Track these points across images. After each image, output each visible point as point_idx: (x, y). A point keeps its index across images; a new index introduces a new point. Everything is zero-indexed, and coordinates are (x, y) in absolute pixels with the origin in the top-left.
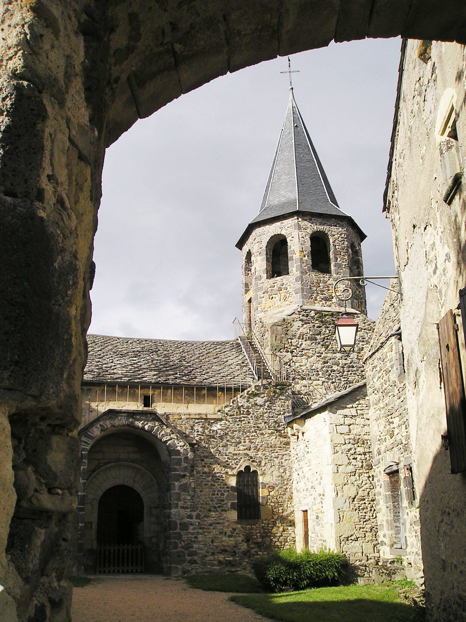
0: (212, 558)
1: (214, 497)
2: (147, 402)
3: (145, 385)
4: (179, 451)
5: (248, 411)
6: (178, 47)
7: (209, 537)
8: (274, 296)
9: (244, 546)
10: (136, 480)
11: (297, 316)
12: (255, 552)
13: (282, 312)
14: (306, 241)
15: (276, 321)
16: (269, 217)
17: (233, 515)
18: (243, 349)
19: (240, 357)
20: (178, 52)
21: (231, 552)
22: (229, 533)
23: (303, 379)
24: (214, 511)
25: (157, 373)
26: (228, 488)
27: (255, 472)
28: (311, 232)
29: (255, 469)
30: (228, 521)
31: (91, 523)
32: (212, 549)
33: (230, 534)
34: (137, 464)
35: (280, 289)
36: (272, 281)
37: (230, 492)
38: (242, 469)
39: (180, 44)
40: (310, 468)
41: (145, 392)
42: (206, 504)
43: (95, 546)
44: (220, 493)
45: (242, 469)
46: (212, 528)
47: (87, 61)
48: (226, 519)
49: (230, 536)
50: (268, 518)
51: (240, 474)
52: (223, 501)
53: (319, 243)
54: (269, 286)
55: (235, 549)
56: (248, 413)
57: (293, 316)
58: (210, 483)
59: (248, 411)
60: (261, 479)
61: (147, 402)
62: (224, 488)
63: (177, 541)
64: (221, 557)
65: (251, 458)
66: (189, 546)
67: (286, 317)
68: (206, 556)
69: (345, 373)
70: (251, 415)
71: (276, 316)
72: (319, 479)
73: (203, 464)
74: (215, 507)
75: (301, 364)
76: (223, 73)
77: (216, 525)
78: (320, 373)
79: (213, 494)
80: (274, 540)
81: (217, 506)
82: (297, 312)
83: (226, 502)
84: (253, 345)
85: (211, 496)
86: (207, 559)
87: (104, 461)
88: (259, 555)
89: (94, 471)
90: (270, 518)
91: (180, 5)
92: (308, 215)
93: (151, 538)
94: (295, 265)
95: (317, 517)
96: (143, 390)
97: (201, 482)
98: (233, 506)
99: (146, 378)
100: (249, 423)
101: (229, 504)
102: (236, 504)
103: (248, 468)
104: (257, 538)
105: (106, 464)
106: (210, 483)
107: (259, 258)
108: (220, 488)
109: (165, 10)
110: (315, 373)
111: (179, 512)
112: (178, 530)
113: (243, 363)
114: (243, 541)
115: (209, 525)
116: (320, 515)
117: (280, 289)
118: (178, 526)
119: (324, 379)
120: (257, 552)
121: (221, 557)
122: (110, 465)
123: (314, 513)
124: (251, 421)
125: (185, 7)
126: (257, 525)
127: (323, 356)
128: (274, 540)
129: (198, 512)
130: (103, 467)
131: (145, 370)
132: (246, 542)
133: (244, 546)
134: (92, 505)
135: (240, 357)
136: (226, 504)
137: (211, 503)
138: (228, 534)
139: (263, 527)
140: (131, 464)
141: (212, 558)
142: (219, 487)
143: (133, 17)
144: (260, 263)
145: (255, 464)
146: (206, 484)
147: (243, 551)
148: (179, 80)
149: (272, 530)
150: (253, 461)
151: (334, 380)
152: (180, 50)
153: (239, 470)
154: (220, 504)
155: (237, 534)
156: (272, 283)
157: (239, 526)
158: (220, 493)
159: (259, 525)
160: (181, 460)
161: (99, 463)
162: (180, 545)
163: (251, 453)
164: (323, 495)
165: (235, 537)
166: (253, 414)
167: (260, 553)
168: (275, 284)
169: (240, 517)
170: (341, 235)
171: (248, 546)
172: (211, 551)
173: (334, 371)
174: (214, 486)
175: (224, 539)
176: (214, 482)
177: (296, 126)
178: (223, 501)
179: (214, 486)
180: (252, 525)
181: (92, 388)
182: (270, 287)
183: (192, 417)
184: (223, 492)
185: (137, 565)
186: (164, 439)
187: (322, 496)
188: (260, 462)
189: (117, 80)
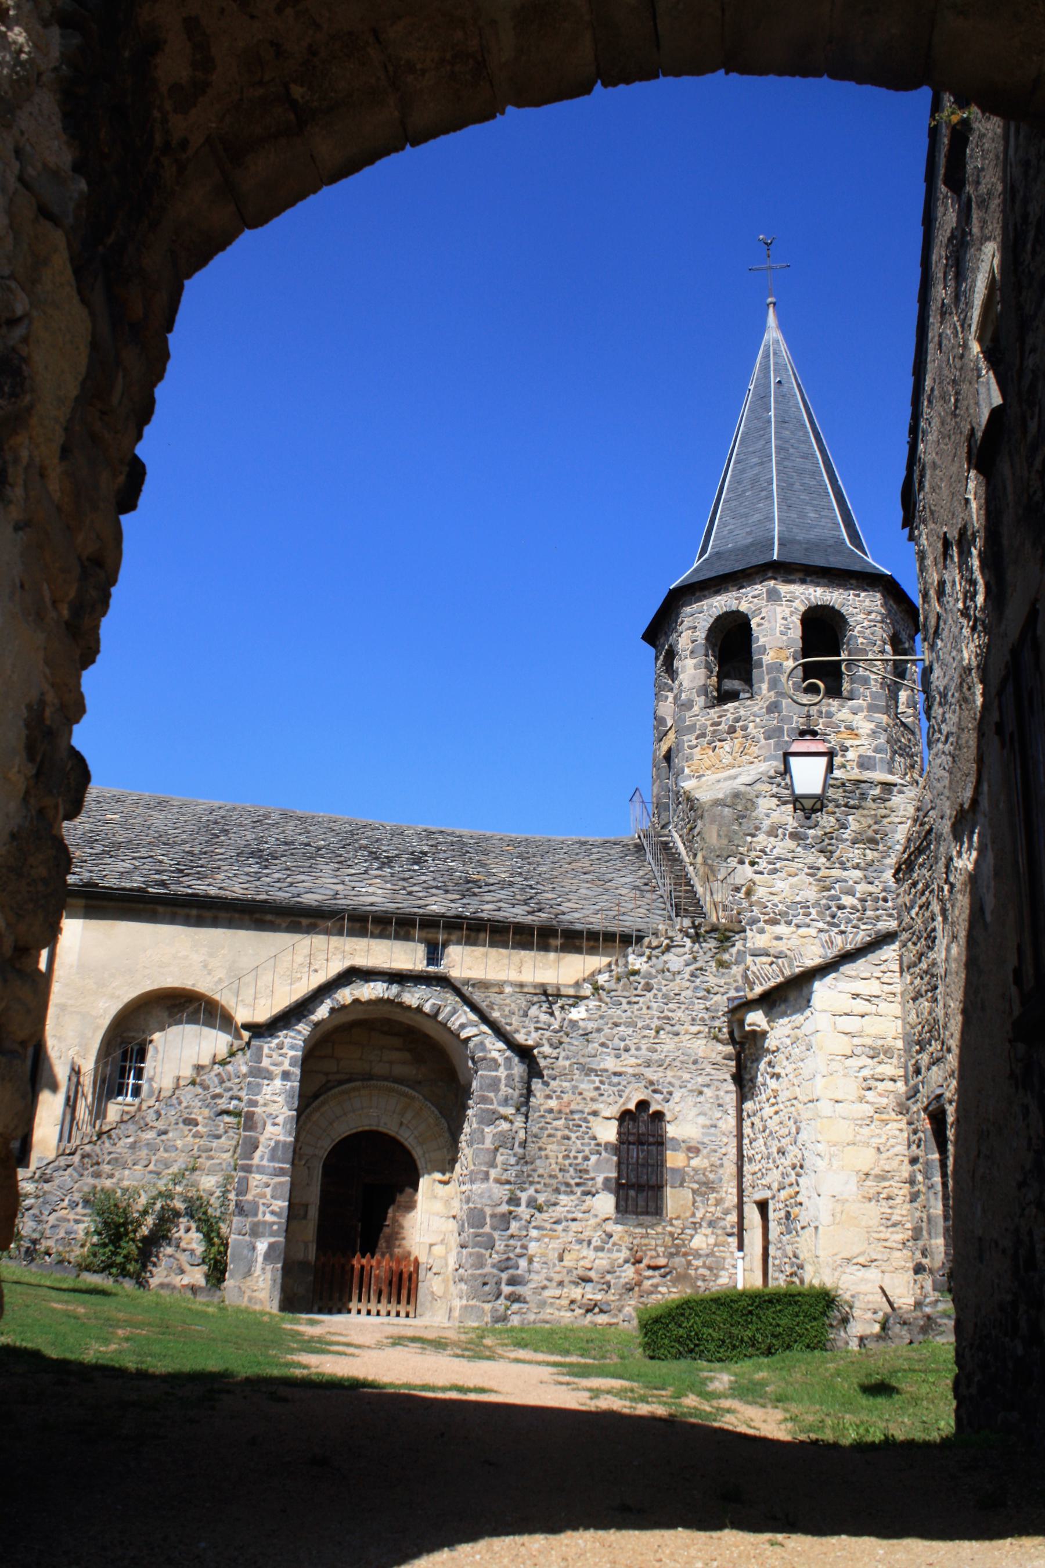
0: (557, 1292)
1: (567, 1162)
2: (434, 955)
3: (430, 923)
4: (495, 1060)
5: (647, 984)
6: (297, 91)
7: (553, 1249)
8: (718, 744)
9: (629, 1273)
10: (405, 1122)
11: (766, 787)
12: (652, 1285)
13: (735, 778)
14: (791, 626)
15: (721, 796)
16: (713, 574)
17: (605, 1203)
18: (649, 856)
19: (641, 873)
20: (300, 100)
21: (598, 1283)
22: (596, 1242)
23: (774, 922)
24: (566, 1193)
25: (458, 897)
26: (599, 1145)
27: (659, 1116)
28: (803, 609)
29: (659, 1108)
30: (596, 1216)
31: (307, 1206)
32: (559, 1273)
33: (599, 1243)
34: (408, 1086)
35: (732, 730)
36: (714, 713)
37: (604, 1153)
38: (632, 1106)
39: (302, 86)
40: (776, 1108)
41: (430, 935)
42: (551, 1176)
43: (312, 1256)
44: (580, 1155)
45: (632, 1106)
46: (559, 1227)
47: (64, 67)
48: (593, 1212)
49: (598, 1249)
50: (683, 1216)
51: (625, 1116)
52: (586, 1171)
53: (822, 630)
54: (709, 723)
55: (609, 1277)
56: (648, 988)
57: (759, 786)
58: (559, 1134)
59: (647, 984)
60: (672, 1131)
61: (434, 955)
62: (590, 1144)
63: (483, 1251)
64: (576, 1293)
65: (652, 1083)
66: (511, 1263)
67: (743, 788)
68: (544, 1288)
69: (869, 913)
70: (654, 991)
71: (721, 785)
72: (793, 1131)
73: (548, 1092)
74: (568, 1185)
75: (773, 890)
76: (399, 148)
77: (570, 1222)
78: (813, 911)
79: (567, 1157)
80: (695, 1263)
81: (573, 1182)
82: (764, 778)
83: (592, 1175)
84: (671, 848)
85: (560, 1160)
86: (547, 1293)
87: (338, 1077)
88: (660, 1292)
89: (316, 1096)
90: (688, 1214)
91: (279, 10)
92: (798, 571)
93: (431, 1245)
94: (766, 678)
95: (788, 1214)
96: (426, 930)
97: (541, 1129)
98: (606, 1186)
99: (434, 907)
100: (648, 1008)
101: (600, 1180)
102: (613, 1181)
103: (643, 1105)
104: (658, 1256)
105: (341, 1083)
106: (559, 1134)
107: (690, 663)
108: (582, 1144)
109: (252, 17)
110: (801, 911)
111: (490, 1190)
112: (487, 1229)
113: (646, 884)
114: (626, 1261)
115: (555, 1223)
116: (795, 1211)
117: (732, 730)
118: (488, 1220)
119: (821, 925)
120: (656, 1286)
121: (576, 1293)
122: (352, 1085)
123: (781, 1206)
124: (655, 1005)
125: (289, 11)
126: (659, 1229)
127: (820, 874)
128: (695, 1263)
129: (531, 1191)
130: (336, 1090)
131: (434, 891)
132: (634, 1264)
133: (629, 1273)
134: (309, 1168)
135: (641, 873)
136: (593, 1179)
137: (560, 1175)
138: (594, 1244)
139: (671, 1234)
140: (396, 1086)
141: (557, 1292)
142: (579, 1142)
143: (191, 25)
144: (692, 671)
145: (658, 1096)
146: (549, 1136)
147: (627, 1283)
148: (312, 156)
149: (690, 1241)
150: (655, 1091)
151: (842, 928)
152: (303, 97)
153: (623, 1108)
154: (581, 1178)
155: (614, 1244)
156: (716, 716)
157: (619, 1228)
158: (580, 1155)
159: (664, 1228)
160: (500, 1080)
161: (328, 1081)
162: (489, 1261)
163: (650, 1073)
164: (802, 1167)
165: (610, 1251)
166: (659, 990)
167: (663, 1289)
168: (723, 719)
169: (623, 1208)
170: (869, 613)
171: (638, 1272)
172: (557, 1278)
173: (843, 907)
174: (568, 1138)
175: (585, 1252)
176: (571, 1131)
177: (779, 382)
178: (586, 1171)
179: (568, 1138)
180: (647, 1227)
181: (320, 922)
182: (712, 725)
183: (526, 990)
184: (587, 1153)
185: (399, 1302)
186: (464, 1035)
187: (798, 1169)
188: (670, 1093)
189: (184, 144)
